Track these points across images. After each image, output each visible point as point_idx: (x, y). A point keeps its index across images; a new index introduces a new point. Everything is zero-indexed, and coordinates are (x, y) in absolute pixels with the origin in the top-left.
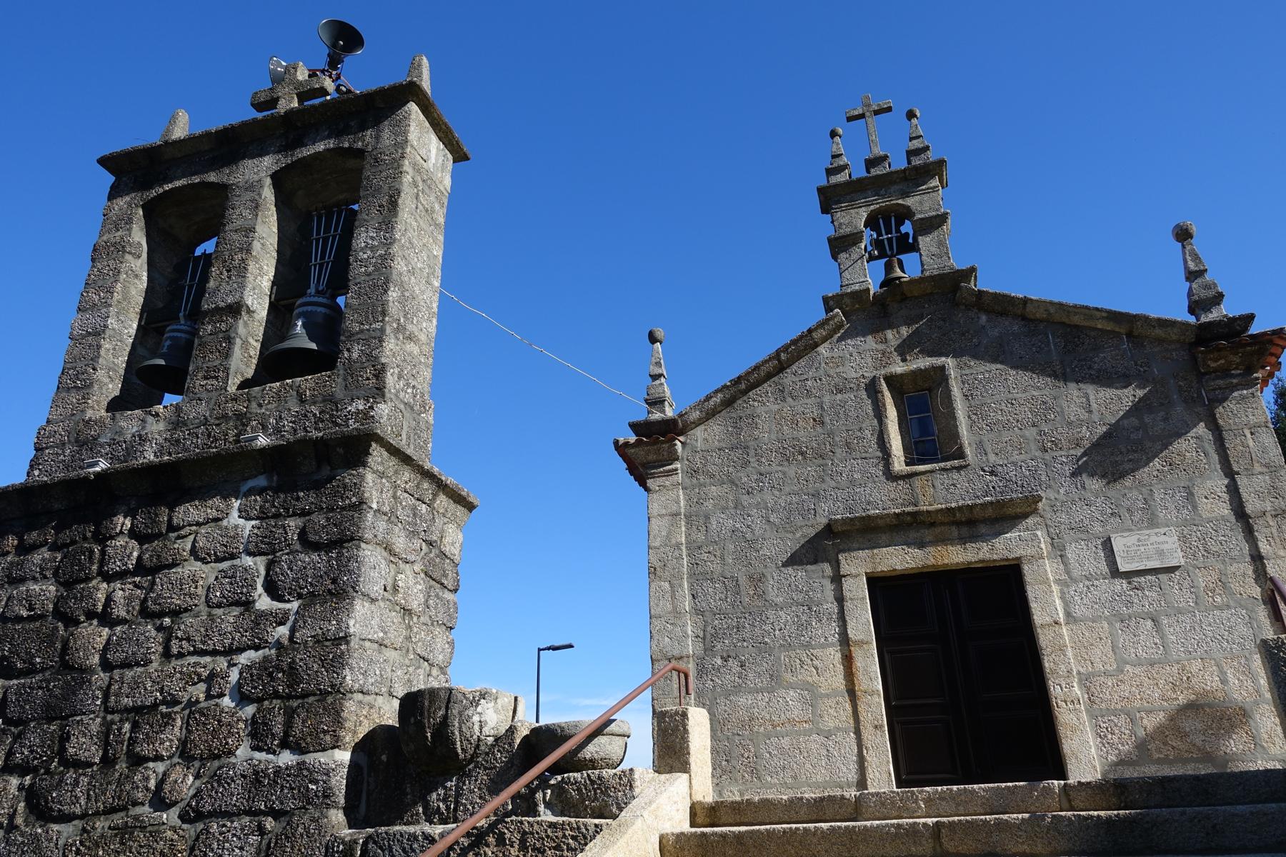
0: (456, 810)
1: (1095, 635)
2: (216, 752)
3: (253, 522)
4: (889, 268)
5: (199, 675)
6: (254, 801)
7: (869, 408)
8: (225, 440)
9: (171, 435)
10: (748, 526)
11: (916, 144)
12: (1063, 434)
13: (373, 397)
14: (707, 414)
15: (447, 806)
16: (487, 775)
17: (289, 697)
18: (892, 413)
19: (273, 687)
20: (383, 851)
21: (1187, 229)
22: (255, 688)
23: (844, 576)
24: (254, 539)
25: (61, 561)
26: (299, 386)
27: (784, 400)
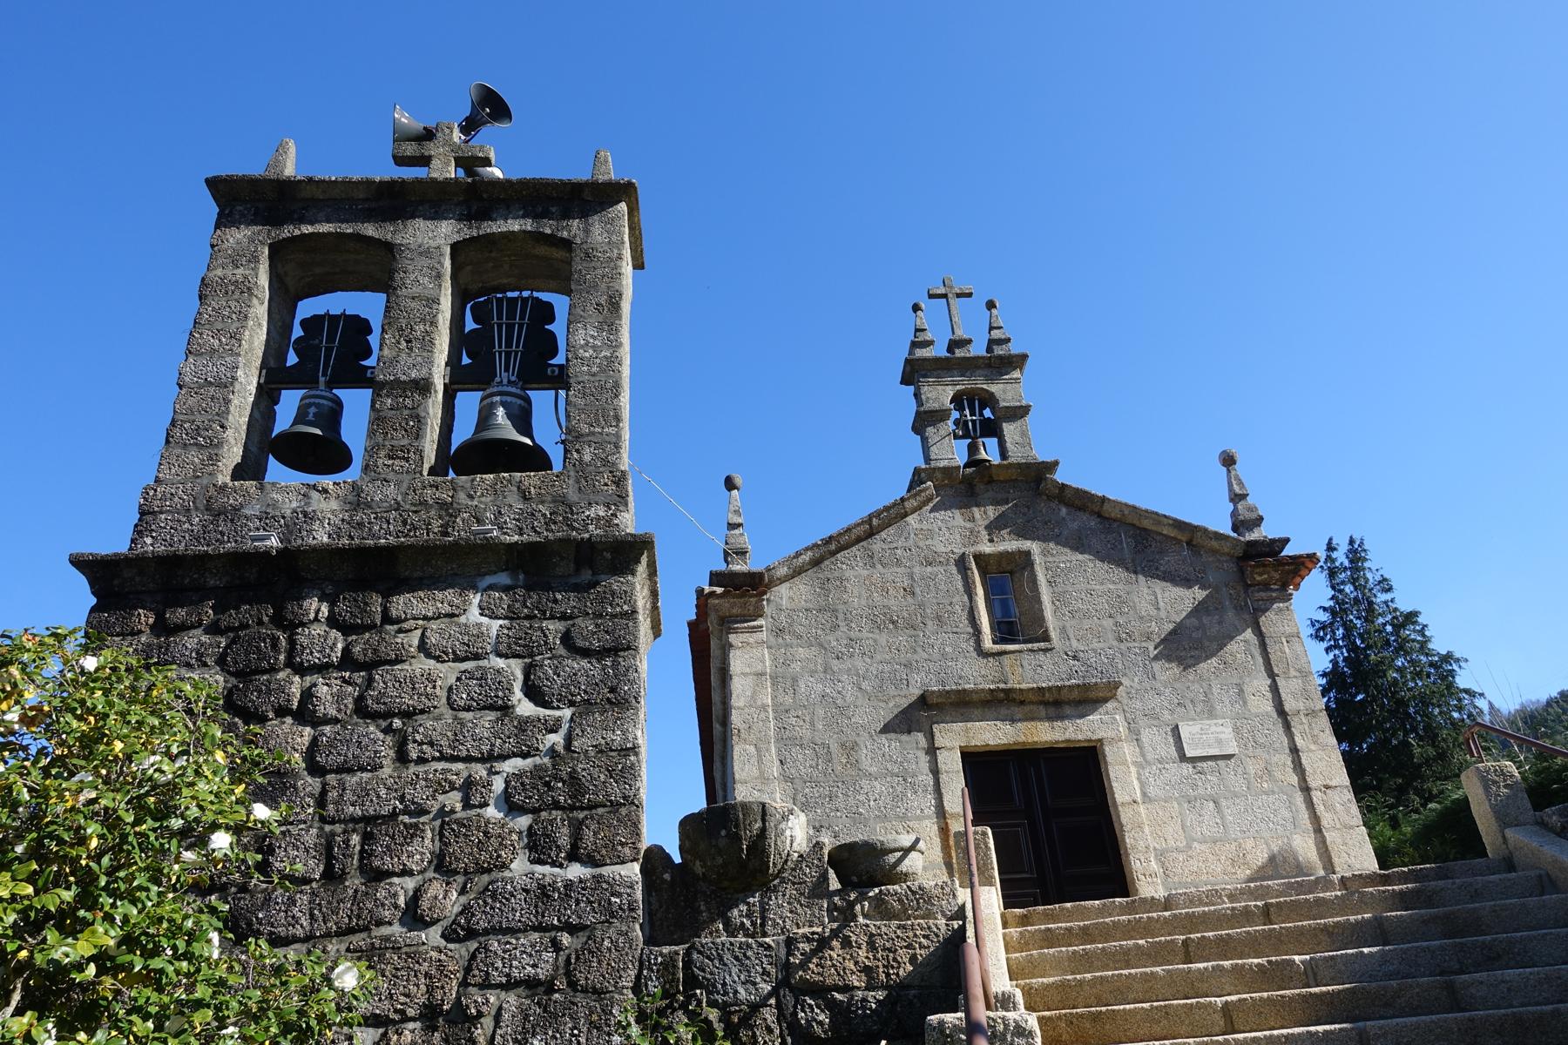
0: (763, 925)
1: (1167, 815)
2: (486, 865)
3: (501, 622)
4: (973, 449)
5: (451, 784)
6: (543, 916)
7: (960, 584)
8: (427, 529)
9: (351, 516)
10: (839, 692)
11: (996, 334)
12: (1135, 626)
13: (615, 504)
14: (794, 571)
15: (752, 922)
16: (796, 889)
17: (572, 808)
18: (980, 591)
19: (553, 797)
20: (712, 960)
21: (1232, 457)
22: (530, 798)
23: (939, 749)
24: (505, 639)
25: (228, 647)
26: (521, 482)
27: (873, 566)
